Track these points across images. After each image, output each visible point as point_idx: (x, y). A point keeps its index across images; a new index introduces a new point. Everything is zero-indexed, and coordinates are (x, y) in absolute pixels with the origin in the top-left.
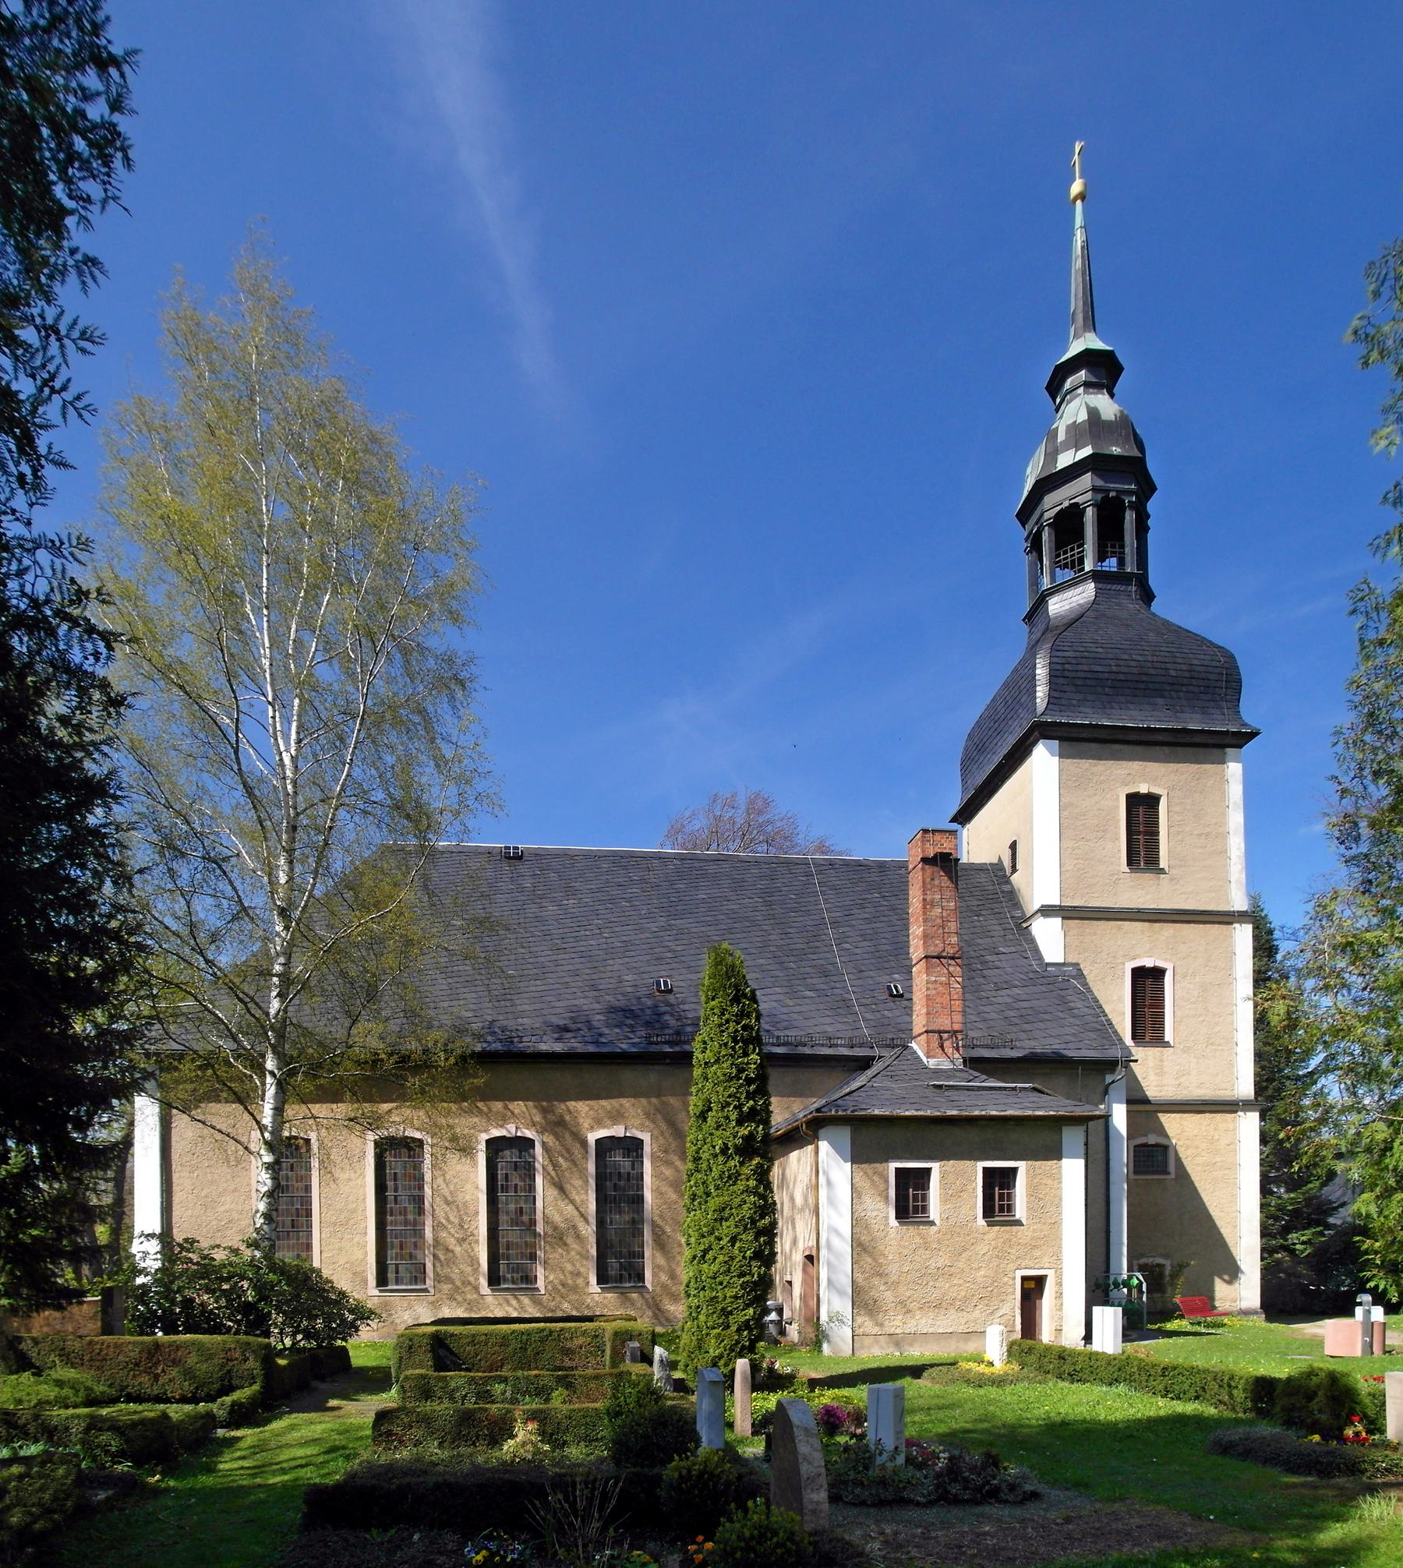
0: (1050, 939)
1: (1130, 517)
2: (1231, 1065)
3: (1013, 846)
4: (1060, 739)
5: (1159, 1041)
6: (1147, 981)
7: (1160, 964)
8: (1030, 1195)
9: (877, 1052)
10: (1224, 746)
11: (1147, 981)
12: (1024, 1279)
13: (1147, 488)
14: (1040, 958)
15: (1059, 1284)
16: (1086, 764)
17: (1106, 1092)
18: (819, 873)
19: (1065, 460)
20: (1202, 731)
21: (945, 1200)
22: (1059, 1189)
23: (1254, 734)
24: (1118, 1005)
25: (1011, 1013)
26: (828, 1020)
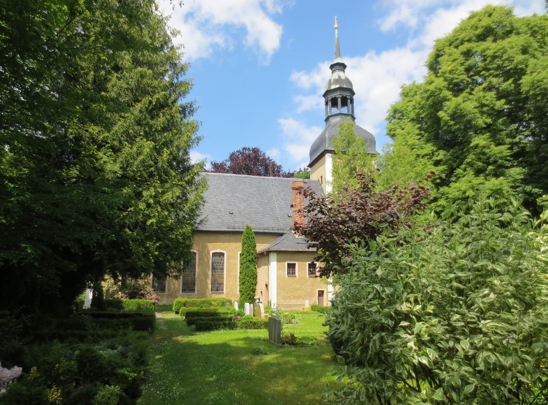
1: (349, 101)
3: (322, 177)
19: (333, 87)
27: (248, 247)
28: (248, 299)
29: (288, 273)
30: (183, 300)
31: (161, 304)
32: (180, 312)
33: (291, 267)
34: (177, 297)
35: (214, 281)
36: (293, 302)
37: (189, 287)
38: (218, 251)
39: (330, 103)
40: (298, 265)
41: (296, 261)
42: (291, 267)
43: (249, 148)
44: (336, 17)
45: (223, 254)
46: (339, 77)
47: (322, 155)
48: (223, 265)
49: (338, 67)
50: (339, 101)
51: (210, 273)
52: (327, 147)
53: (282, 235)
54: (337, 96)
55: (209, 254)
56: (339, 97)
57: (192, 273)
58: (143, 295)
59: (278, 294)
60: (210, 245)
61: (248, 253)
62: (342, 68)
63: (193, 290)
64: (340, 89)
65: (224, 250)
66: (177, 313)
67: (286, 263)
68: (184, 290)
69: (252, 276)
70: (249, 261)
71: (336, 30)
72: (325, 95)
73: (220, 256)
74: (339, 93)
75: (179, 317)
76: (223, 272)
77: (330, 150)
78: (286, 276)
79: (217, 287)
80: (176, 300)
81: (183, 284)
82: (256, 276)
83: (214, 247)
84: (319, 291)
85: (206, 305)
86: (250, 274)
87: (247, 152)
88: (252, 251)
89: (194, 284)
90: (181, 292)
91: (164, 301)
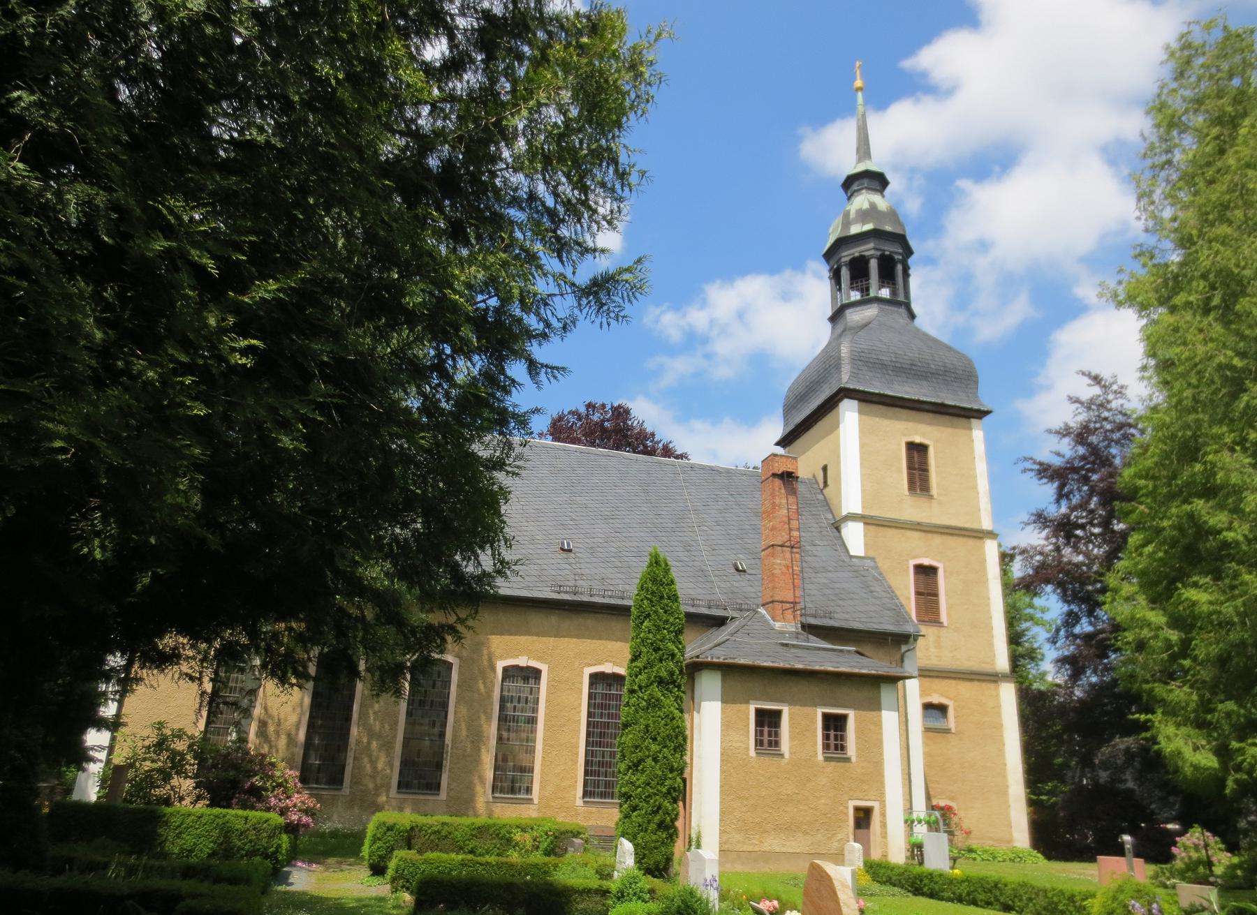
0: (855, 538)
1: (899, 267)
2: (991, 645)
3: (825, 469)
4: (860, 400)
5: (936, 622)
6: (926, 573)
7: (934, 563)
8: (857, 738)
9: (730, 613)
10: (969, 417)
11: (926, 573)
12: (596, 678)
13: (908, 252)
14: (847, 551)
15: (883, 815)
16: (877, 420)
17: (902, 661)
18: (684, 472)
19: (855, 229)
20: (955, 407)
21: (792, 738)
22: (881, 734)
23: (988, 413)
24: (906, 589)
25: (828, 592)
26: (691, 585)
27: (659, 629)
28: (653, 826)
29: (759, 743)
30: (406, 818)
31: (327, 827)
32: (390, 872)
33: (768, 720)
34: (379, 808)
35: (505, 760)
36: (774, 843)
37: (421, 774)
38: (522, 661)
39: (845, 274)
40: (791, 719)
41: (782, 701)
42: (768, 720)
43: (603, 406)
44: (858, 64)
45: (536, 674)
46: (873, 206)
47: (829, 405)
48: (535, 710)
49: (866, 182)
50: (873, 264)
51: (492, 730)
52: (845, 378)
53: (720, 622)
54: (866, 254)
55: (493, 668)
56: (872, 257)
57: (436, 730)
58: (257, 794)
59: (723, 813)
60: (497, 643)
61: (657, 650)
62: (876, 185)
63: (434, 787)
64: (876, 234)
65: (539, 659)
66: (378, 870)
67: (752, 709)
68: (403, 785)
69: (669, 737)
70: (661, 682)
71: (860, 94)
72: (829, 255)
73: (526, 679)
74: (871, 245)
75: (379, 888)
76: (534, 731)
77: (854, 391)
78: (752, 753)
79: (512, 779)
80: (378, 817)
81: (404, 763)
82: (685, 739)
83: (509, 650)
84: (857, 809)
85: (488, 844)
86: (664, 732)
87: (597, 415)
88: (671, 646)
89: (439, 766)
90: (393, 791)
91: (335, 822)
